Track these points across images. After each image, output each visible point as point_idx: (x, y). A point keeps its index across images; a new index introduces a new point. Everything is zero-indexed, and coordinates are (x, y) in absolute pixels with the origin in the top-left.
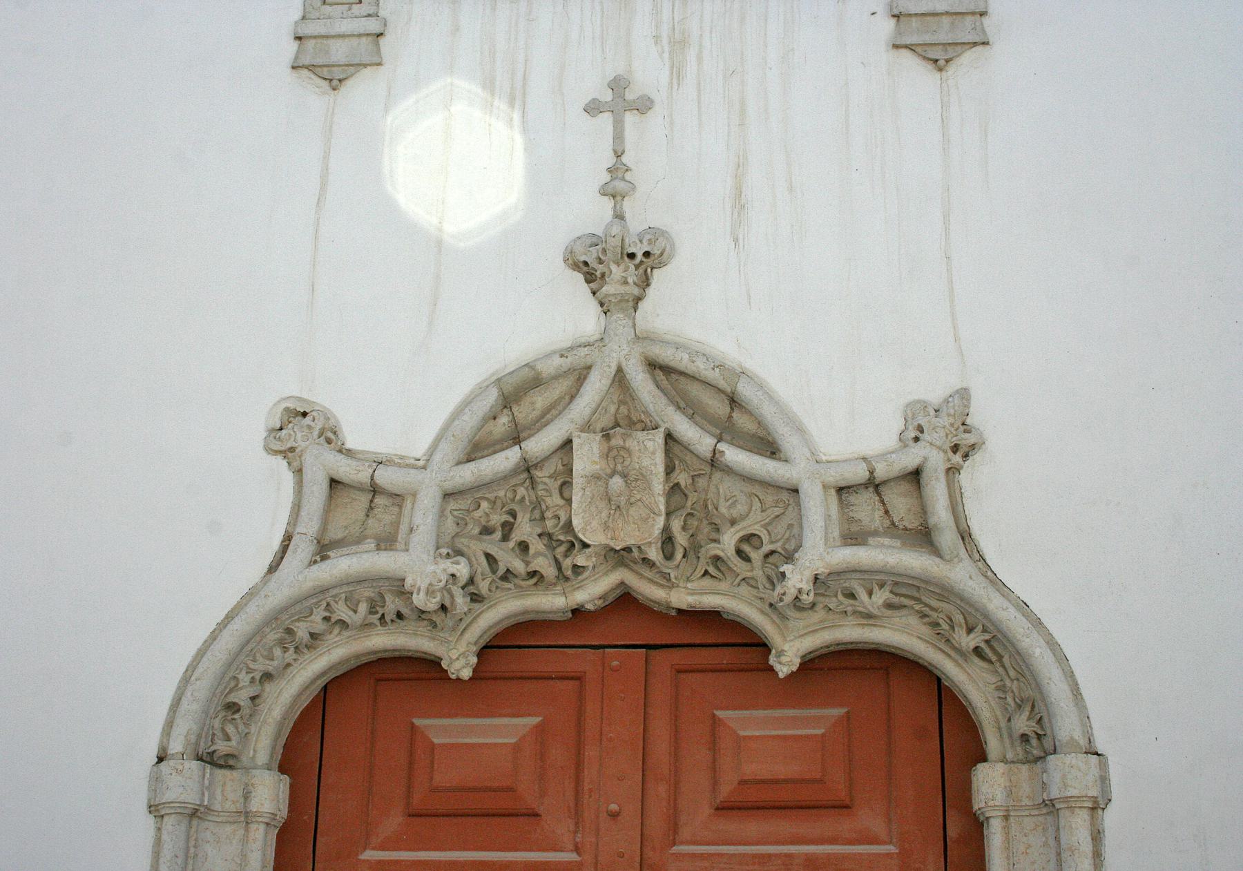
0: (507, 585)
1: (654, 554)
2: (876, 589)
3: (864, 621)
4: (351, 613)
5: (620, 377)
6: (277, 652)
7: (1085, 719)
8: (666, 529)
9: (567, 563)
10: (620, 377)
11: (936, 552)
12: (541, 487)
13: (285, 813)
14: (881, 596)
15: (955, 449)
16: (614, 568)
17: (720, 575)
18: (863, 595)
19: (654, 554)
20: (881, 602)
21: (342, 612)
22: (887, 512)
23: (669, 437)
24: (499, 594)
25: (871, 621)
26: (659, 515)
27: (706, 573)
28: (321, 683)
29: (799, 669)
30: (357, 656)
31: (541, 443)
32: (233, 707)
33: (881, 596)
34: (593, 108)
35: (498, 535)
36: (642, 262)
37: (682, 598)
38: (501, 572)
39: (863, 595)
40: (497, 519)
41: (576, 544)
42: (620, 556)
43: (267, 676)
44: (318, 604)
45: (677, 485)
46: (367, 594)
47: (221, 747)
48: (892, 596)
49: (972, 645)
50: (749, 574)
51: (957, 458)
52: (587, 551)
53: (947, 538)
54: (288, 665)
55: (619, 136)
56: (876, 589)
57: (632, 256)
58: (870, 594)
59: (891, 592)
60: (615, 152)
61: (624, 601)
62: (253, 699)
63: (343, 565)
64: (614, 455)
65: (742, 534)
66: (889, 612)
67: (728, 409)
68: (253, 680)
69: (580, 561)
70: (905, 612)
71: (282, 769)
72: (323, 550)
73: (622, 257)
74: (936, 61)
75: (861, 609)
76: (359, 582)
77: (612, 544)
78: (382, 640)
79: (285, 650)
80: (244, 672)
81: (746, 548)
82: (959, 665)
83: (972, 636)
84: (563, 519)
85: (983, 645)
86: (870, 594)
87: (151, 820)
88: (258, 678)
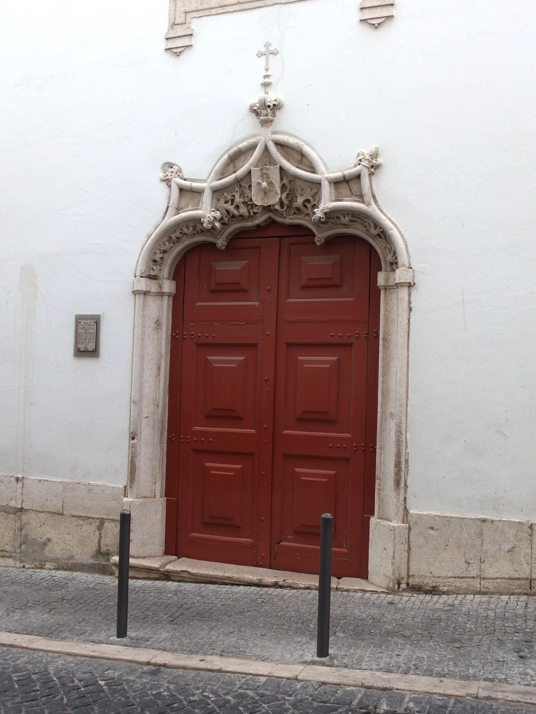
0: (234, 219)
1: (277, 207)
2: (346, 216)
3: (344, 226)
4: (187, 231)
5: (266, 149)
6: (167, 244)
7: (409, 256)
8: (281, 199)
9: (251, 211)
10: (266, 149)
11: (363, 202)
12: (243, 187)
13: (175, 292)
14: (347, 219)
15: (372, 167)
16: (267, 212)
17: (299, 213)
18: (342, 218)
19: (277, 207)
20: (348, 220)
21: (185, 230)
22: (350, 190)
23: (281, 169)
24: (233, 222)
25: (347, 226)
26: (278, 194)
27: (295, 213)
28: (183, 252)
29: (324, 243)
30: (193, 244)
31: (241, 172)
32: (155, 261)
33: (347, 219)
34: (260, 55)
35: (230, 202)
36: (273, 108)
37: (288, 221)
38: (231, 215)
39: (342, 218)
40: (229, 197)
41: (254, 206)
42: (268, 209)
43: (165, 252)
44: (178, 228)
45: (284, 184)
46: (192, 224)
47: (152, 273)
48: (351, 218)
49: (376, 233)
50: (307, 212)
51: (372, 170)
52: (257, 207)
53: (368, 197)
54: (171, 247)
55: (267, 63)
56: (346, 216)
57: (269, 106)
58: (345, 217)
59: (351, 216)
60: (266, 69)
61: (272, 223)
62: (161, 258)
63: (183, 215)
64: (265, 176)
65: (304, 199)
66: (351, 223)
67: (301, 157)
68: (160, 253)
69: (255, 211)
70: (356, 223)
71: (174, 278)
72: (178, 210)
73: (266, 108)
74: (374, 24)
75: (342, 223)
76: (189, 221)
77: (264, 205)
78: (198, 239)
79: (170, 243)
80: (158, 250)
81: (306, 204)
82: (374, 240)
83: (376, 230)
84: (250, 197)
85: (380, 233)
86: (345, 217)
87: (133, 295)
88: (162, 252)
